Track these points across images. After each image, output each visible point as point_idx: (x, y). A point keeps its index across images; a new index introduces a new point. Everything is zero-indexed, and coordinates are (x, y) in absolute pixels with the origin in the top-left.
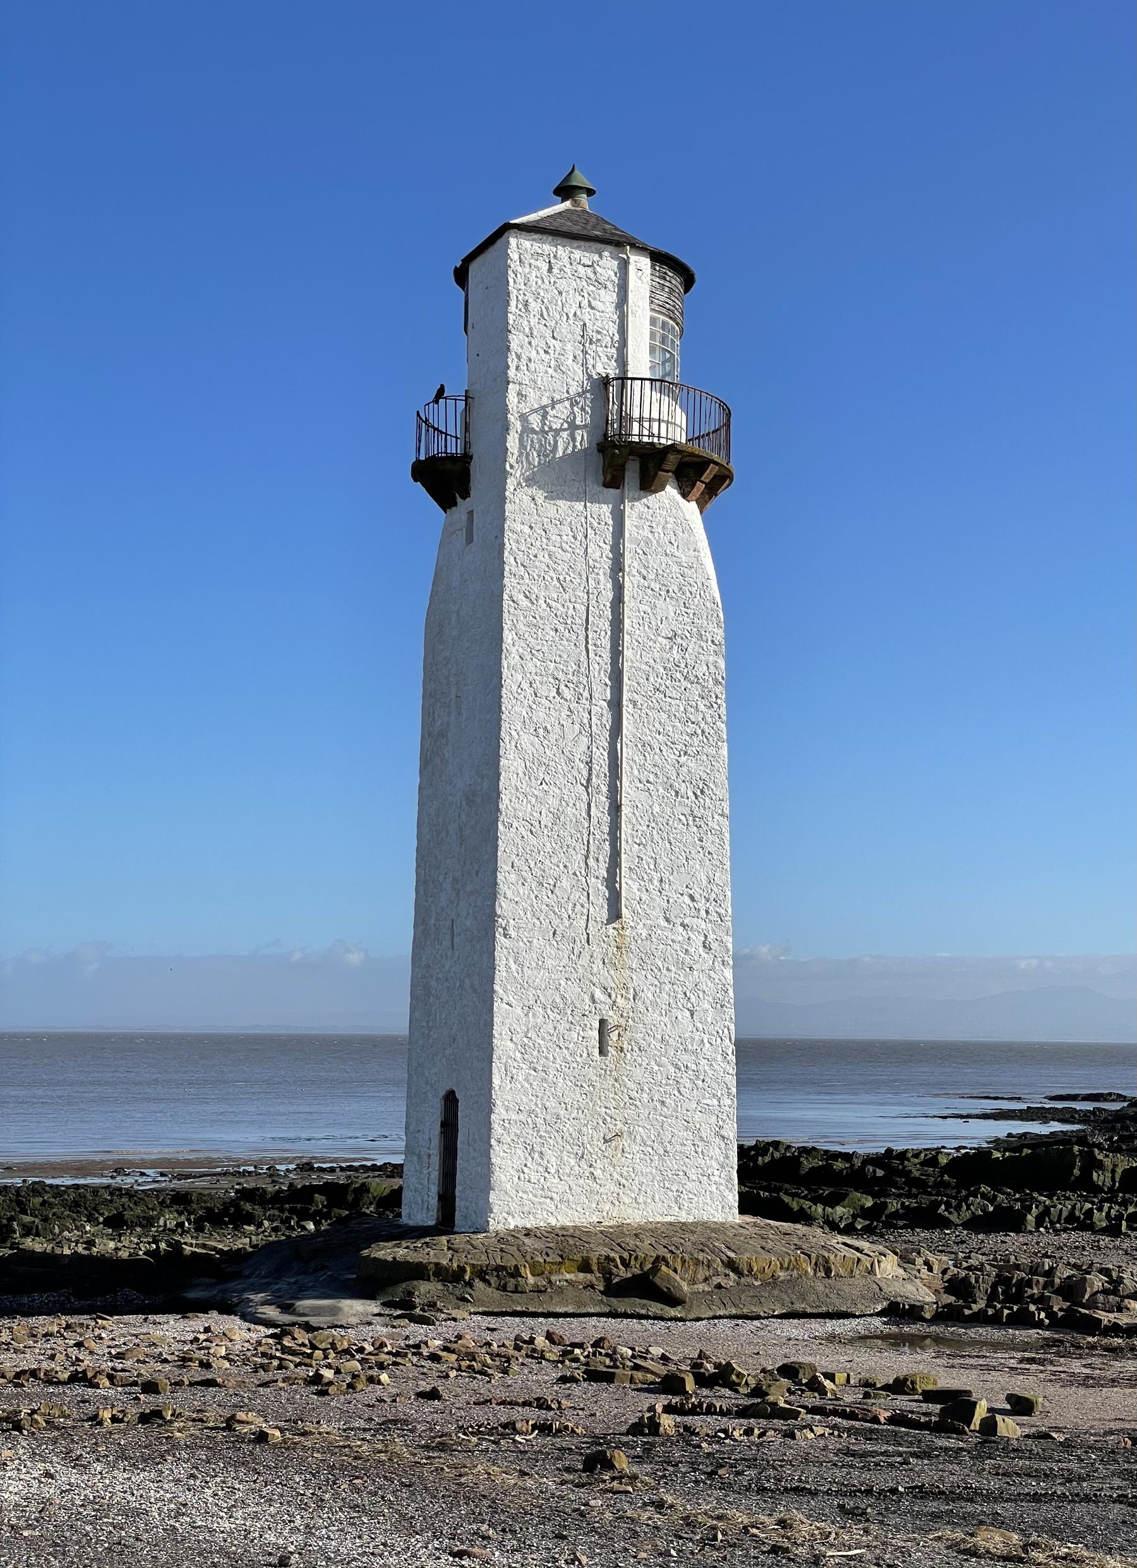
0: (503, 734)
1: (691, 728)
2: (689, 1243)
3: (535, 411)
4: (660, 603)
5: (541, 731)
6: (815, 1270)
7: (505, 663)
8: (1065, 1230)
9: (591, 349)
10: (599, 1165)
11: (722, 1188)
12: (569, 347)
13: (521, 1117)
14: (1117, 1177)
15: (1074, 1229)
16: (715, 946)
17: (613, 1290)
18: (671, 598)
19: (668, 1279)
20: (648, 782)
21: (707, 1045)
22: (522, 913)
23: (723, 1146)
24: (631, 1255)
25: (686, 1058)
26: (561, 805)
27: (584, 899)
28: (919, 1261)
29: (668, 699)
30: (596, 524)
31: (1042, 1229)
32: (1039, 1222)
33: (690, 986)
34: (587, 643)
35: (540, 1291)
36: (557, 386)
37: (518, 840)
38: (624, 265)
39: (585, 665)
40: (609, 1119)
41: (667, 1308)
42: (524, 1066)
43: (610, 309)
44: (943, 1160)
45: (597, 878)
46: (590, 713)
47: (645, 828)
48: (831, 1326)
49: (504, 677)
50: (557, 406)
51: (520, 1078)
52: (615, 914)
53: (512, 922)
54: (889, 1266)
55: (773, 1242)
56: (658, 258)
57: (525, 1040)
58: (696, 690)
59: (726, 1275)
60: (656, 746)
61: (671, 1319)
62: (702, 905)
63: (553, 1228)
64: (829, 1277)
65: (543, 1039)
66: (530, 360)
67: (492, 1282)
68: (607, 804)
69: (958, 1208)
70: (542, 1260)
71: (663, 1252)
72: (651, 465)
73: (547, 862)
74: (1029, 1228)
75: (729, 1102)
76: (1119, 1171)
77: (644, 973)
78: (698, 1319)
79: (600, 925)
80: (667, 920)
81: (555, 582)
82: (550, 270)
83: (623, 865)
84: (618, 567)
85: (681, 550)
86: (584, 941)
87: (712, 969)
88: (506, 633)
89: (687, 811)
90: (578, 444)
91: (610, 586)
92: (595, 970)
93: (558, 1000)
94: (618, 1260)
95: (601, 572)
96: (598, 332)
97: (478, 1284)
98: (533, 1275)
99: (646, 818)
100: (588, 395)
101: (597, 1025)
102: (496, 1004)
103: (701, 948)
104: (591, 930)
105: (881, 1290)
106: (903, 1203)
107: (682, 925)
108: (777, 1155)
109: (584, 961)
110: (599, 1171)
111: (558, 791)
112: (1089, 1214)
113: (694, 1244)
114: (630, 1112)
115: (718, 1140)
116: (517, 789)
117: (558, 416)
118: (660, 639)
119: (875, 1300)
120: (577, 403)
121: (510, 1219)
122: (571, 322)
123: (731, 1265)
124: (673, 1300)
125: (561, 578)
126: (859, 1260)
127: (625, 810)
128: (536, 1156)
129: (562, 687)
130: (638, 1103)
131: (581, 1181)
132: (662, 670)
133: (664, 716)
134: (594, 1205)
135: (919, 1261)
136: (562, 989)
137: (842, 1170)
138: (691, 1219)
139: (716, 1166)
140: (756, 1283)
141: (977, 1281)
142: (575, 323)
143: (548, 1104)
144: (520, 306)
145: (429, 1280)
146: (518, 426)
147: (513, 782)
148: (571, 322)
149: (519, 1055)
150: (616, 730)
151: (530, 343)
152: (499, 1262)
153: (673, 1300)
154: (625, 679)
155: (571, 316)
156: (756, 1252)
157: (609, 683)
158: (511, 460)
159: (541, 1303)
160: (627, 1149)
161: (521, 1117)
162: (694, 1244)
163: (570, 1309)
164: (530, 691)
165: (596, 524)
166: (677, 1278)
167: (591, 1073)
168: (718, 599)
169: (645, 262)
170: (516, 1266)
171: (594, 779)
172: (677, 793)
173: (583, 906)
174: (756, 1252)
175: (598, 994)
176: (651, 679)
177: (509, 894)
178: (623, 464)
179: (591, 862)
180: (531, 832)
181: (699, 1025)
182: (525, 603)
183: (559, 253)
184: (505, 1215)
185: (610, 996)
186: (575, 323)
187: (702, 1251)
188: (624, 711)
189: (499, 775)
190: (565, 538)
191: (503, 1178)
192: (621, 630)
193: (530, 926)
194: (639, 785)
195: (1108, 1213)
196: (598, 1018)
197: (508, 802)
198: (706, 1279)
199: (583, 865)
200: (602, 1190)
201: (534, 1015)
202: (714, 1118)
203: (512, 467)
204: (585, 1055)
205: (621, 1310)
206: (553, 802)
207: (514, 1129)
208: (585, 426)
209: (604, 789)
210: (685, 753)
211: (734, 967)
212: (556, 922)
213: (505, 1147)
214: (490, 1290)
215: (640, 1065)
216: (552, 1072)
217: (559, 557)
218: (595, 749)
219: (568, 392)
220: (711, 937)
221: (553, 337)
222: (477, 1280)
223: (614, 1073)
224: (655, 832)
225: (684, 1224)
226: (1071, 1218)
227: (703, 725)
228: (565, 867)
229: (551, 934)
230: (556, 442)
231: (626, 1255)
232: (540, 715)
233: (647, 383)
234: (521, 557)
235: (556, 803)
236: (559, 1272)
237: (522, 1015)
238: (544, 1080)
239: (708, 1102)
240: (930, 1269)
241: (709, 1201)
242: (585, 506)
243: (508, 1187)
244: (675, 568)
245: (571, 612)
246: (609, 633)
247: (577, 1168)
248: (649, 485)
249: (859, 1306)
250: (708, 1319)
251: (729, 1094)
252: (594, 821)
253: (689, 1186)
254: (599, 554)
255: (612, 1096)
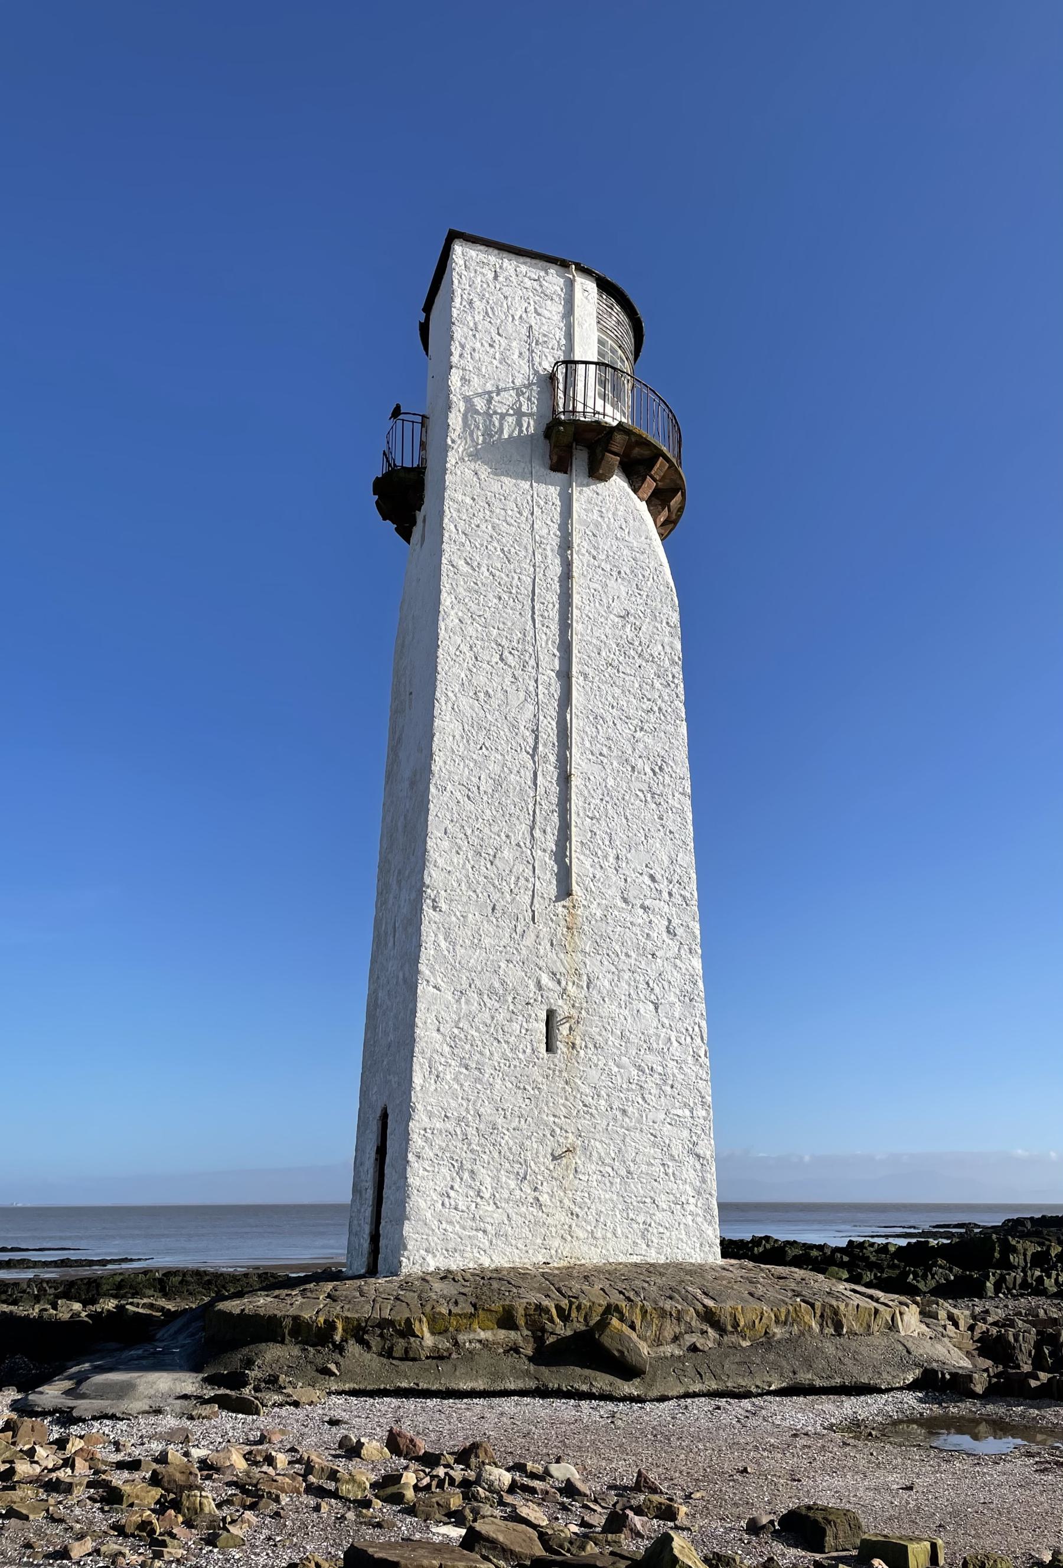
0: (438, 695)
1: (647, 705)
2: (654, 1288)
3: (479, 395)
4: (611, 583)
5: (481, 695)
6: (821, 1325)
7: (442, 625)
8: (1022, 1295)
9: (538, 349)
10: (546, 1188)
11: (699, 1220)
12: (514, 344)
13: (449, 1126)
14: (1029, 1259)
15: (1029, 1295)
16: (680, 931)
17: (548, 1354)
18: (623, 579)
19: (621, 1337)
20: (601, 754)
21: (675, 1044)
22: (455, 885)
23: (698, 1167)
24: (571, 1303)
25: (651, 1059)
26: (503, 771)
27: (528, 872)
28: (942, 1314)
29: (621, 674)
30: (542, 503)
31: (1001, 1295)
32: (997, 1288)
33: (654, 975)
34: (533, 613)
35: (441, 1358)
36: (503, 375)
37: (452, 804)
38: (570, 284)
39: (532, 633)
40: (558, 1131)
41: (619, 1382)
42: (453, 1063)
43: (557, 318)
44: (892, 1249)
45: (544, 851)
46: (536, 681)
47: (598, 801)
48: (851, 1406)
49: (441, 637)
50: (502, 394)
51: (448, 1077)
52: (565, 891)
53: (443, 892)
54: (911, 1320)
55: (761, 1298)
56: (605, 286)
57: (456, 1031)
58: (651, 670)
59: (704, 1332)
60: (609, 718)
61: (623, 1399)
62: (663, 886)
63: (483, 1270)
64: (840, 1335)
65: (478, 1030)
66: (474, 350)
67: (373, 1344)
68: (556, 774)
69: (924, 1277)
70: (445, 1311)
71: (616, 1299)
72: (598, 450)
73: (486, 830)
74: (990, 1294)
75: (704, 1113)
76: (1029, 1254)
77: (599, 958)
78: (663, 1399)
79: (547, 902)
80: (625, 901)
81: (499, 552)
82: (496, 277)
83: (574, 839)
84: (566, 545)
85: (632, 537)
86: (529, 919)
87: (678, 957)
88: (444, 595)
89: (645, 787)
90: (524, 429)
91: (558, 561)
92: (542, 952)
93: (497, 985)
94: (554, 1311)
95: (548, 547)
96: (545, 335)
97: (353, 1348)
98: (433, 1333)
99: (599, 791)
100: (535, 387)
101: (544, 1016)
102: (420, 987)
103: (665, 935)
104: (536, 905)
105: (909, 1352)
106: (875, 1275)
107: (643, 907)
108: (768, 1246)
109: (529, 940)
110: (546, 1196)
111: (500, 757)
112: (1040, 1280)
113: (661, 1289)
114: (585, 1122)
115: (692, 1159)
116: (453, 751)
117: (505, 401)
118: (612, 616)
119: (903, 1367)
120: (523, 394)
121: (429, 1259)
122: (517, 323)
123: (709, 1317)
124: (627, 1370)
125: (506, 549)
126: (877, 1311)
127: (576, 782)
128: (466, 1176)
129: (506, 653)
130: (594, 1111)
131: (523, 1209)
132: (614, 646)
133: (617, 691)
134: (539, 1241)
135: (942, 1314)
136: (501, 972)
137: (817, 1257)
138: (662, 1260)
139: (690, 1191)
140: (745, 1344)
141: (1016, 1340)
142: (517, 326)
143: (482, 1110)
144: (464, 303)
145: (282, 1342)
146: (462, 406)
147: (448, 744)
148: (517, 323)
149: (447, 1049)
150: (565, 700)
151: (474, 336)
152: (386, 1314)
153: (627, 1370)
154: (575, 651)
155: (517, 318)
156: (742, 1300)
157: (558, 654)
158: (453, 435)
159: (439, 1375)
160: (581, 1168)
161: (449, 1126)
162: (661, 1289)
163: (480, 1385)
164: (469, 654)
165: (542, 503)
166: (634, 1336)
167: (535, 1073)
168: (672, 584)
169: (592, 286)
170: (408, 1320)
171: (541, 748)
172: (633, 768)
173: (527, 880)
174: (742, 1300)
175: (545, 979)
176: (603, 654)
177: (441, 862)
178: (571, 447)
179: (537, 833)
180: (468, 797)
181: (666, 1021)
182: (465, 569)
183: (505, 265)
184: (423, 1252)
185: (559, 983)
186: (517, 326)
187: (671, 1298)
188: (574, 682)
189: (433, 735)
190: (510, 512)
191: (422, 1204)
192: (570, 604)
193: (464, 899)
194: (590, 757)
195: (1056, 1280)
196: (546, 1008)
197: (441, 764)
198: (676, 1339)
199: (528, 836)
200: (550, 1220)
201: (467, 1002)
202: (686, 1133)
203: (453, 441)
204: (529, 1051)
205: (553, 1385)
206: (495, 768)
207: (439, 1141)
208: (531, 415)
209: (553, 759)
210: (642, 729)
211: (702, 957)
212: (496, 896)
213: (426, 1164)
214: (368, 1356)
215: (596, 1065)
216: (488, 1071)
217: (503, 529)
218: (541, 718)
219: (513, 382)
220: (676, 922)
221: (499, 334)
222: (351, 1342)
223: (565, 1074)
224: (609, 807)
225: (652, 1265)
226: (1025, 1285)
227: (659, 702)
228: (507, 836)
229: (490, 909)
230: (501, 425)
231: (564, 1303)
232: (481, 679)
233: (592, 367)
234: (461, 525)
235: (497, 769)
236: (469, 1328)
237: (453, 1001)
238: (478, 1080)
239: (680, 1112)
240: (956, 1325)
241: (684, 1236)
242: (531, 486)
243: (429, 1215)
244: (626, 552)
245: (516, 581)
246: (557, 606)
247: (518, 1192)
248: (596, 473)
249: (885, 1375)
250: (678, 1397)
251: (703, 1103)
252: (541, 790)
253: (659, 1216)
254: (546, 531)
255: (562, 1101)
